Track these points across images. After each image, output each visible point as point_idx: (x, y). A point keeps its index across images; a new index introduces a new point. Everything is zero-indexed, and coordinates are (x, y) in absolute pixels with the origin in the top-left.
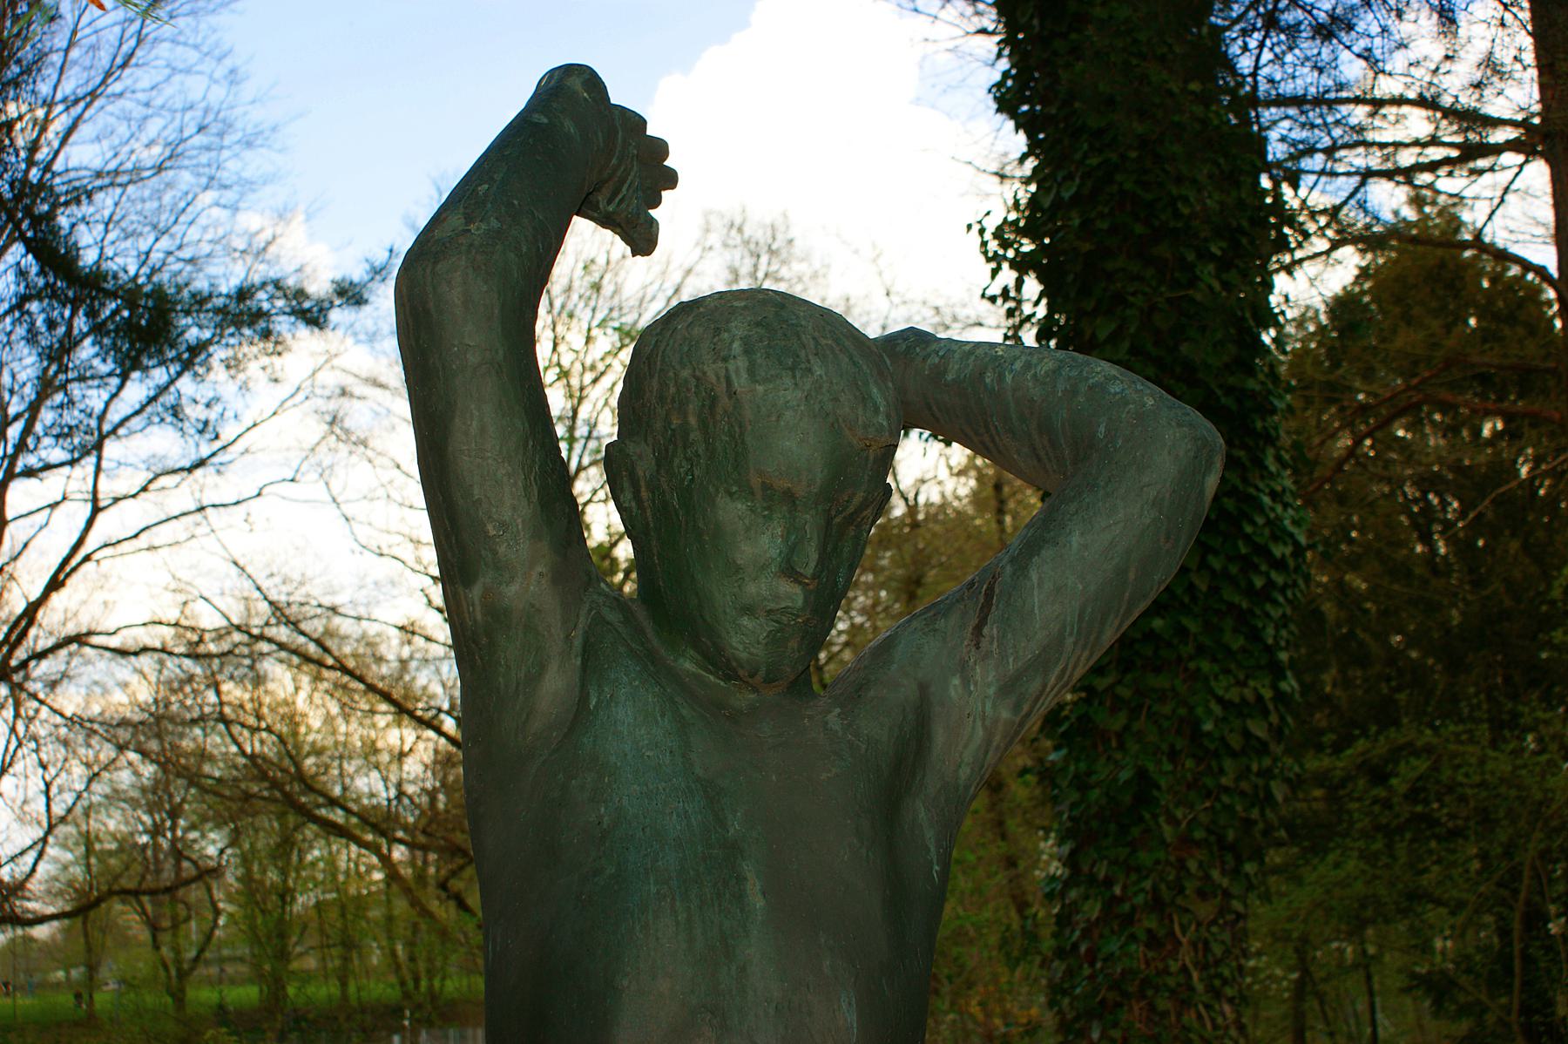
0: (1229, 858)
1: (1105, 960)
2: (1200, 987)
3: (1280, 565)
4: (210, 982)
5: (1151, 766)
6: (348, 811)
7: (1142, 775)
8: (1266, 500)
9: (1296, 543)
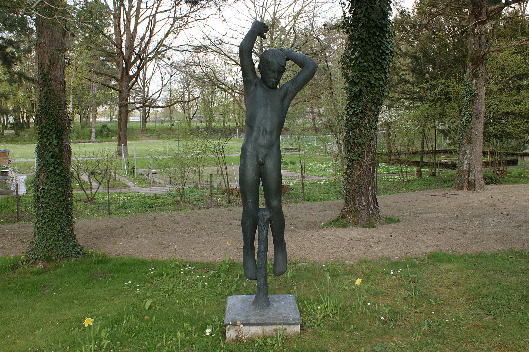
0: (375, 105)
1: (353, 121)
2: (368, 126)
3: (387, 54)
4: (196, 122)
5: (362, 89)
6: (225, 85)
7: (360, 90)
8: (386, 43)
9: (391, 51)
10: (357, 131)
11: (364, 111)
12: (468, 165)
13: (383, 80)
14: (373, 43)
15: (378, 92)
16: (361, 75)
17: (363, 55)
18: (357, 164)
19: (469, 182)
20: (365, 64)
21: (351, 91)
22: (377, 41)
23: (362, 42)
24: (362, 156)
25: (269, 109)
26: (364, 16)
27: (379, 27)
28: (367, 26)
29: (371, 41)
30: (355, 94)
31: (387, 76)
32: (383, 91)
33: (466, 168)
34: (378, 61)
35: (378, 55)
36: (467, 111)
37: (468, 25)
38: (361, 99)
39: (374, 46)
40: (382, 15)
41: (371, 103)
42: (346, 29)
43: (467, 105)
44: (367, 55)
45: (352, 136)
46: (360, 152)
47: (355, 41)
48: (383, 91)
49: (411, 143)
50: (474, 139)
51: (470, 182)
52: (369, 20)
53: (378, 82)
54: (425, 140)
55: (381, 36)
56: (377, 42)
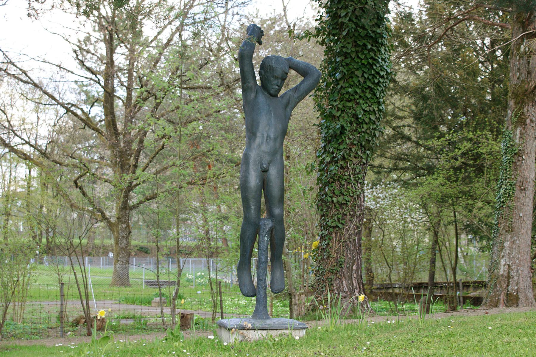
0: (363, 149)
3: (382, 77)
5: (345, 125)
7: (342, 127)
8: (380, 60)
9: (387, 72)
10: (336, 186)
11: (346, 157)
12: (507, 267)
13: (375, 114)
14: (362, 59)
15: (368, 131)
16: (344, 106)
17: (347, 78)
18: (336, 233)
19: (508, 295)
20: (350, 90)
21: (328, 128)
22: (368, 57)
23: (346, 58)
24: (343, 222)
25: (273, 115)
26: (350, 20)
27: (371, 37)
28: (354, 35)
29: (359, 57)
30: (335, 132)
31: (380, 107)
32: (375, 129)
33: (504, 271)
34: (369, 87)
35: (368, 78)
36: (506, 179)
37: (511, 39)
38: (343, 141)
39: (363, 64)
40: (375, 20)
41: (358, 145)
42: (321, 39)
43: (506, 169)
44: (352, 77)
45: (329, 192)
46: (340, 216)
47: (334, 57)
48: (375, 129)
49: (411, 272)
50: (516, 225)
51: (510, 294)
52: (357, 27)
53: (368, 116)
54: (437, 248)
55: (373, 50)
56: (367, 59)
